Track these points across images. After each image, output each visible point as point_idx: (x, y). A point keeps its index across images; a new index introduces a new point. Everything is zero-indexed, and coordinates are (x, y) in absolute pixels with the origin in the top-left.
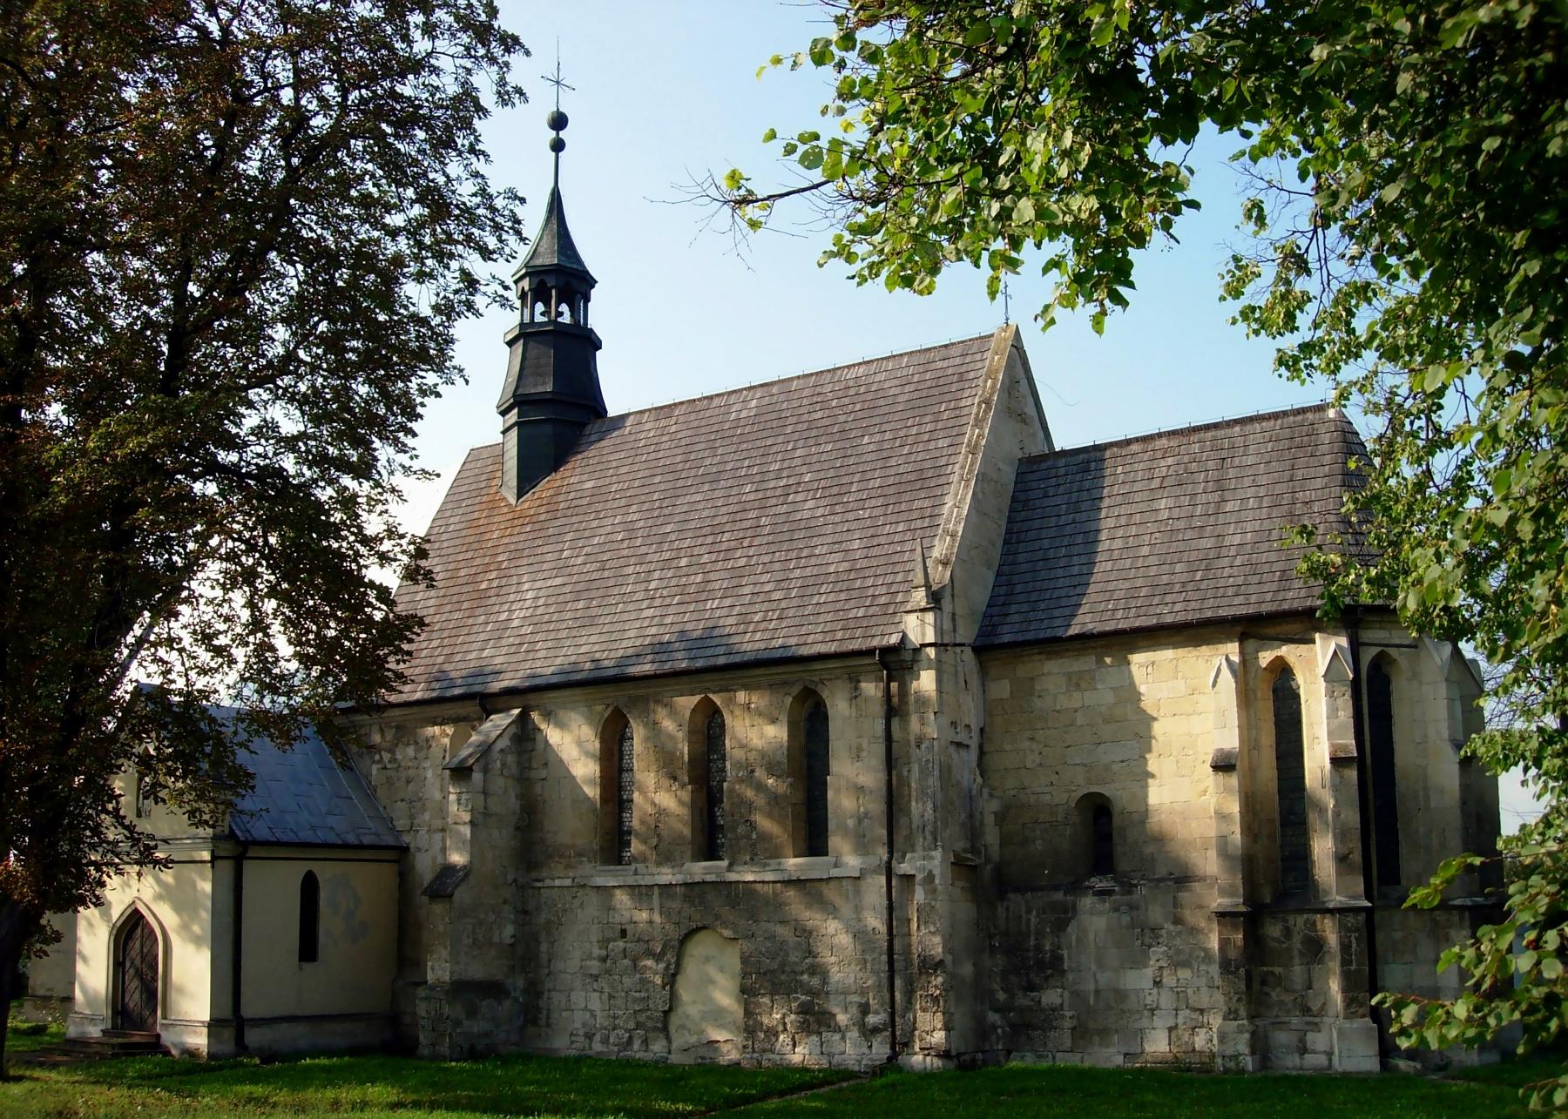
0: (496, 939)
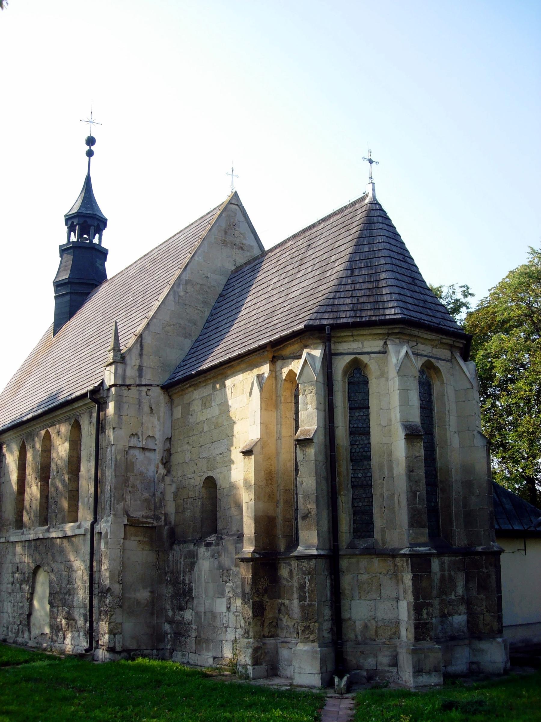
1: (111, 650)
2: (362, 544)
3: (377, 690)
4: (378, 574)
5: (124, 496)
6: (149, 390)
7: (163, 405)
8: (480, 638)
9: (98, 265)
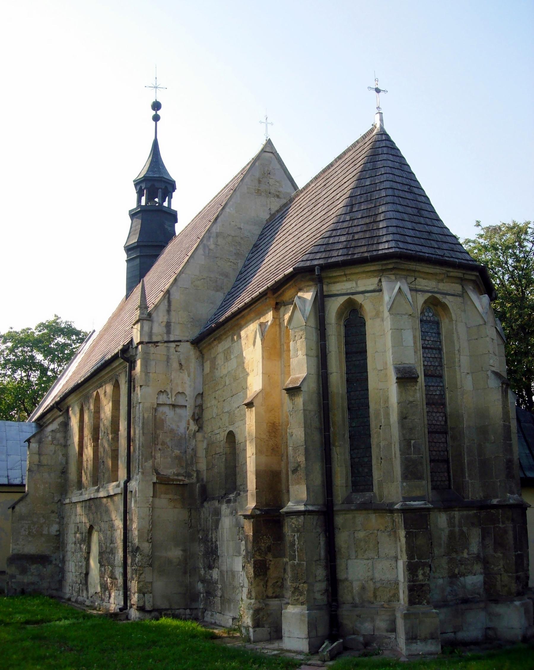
0: (45, 532)
1: (141, 609)
2: (359, 498)
3: (366, 659)
4: (376, 531)
5: (153, 454)
6: (178, 346)
7: (193, 361)
8: (496, 601)
9: (166, 227)
